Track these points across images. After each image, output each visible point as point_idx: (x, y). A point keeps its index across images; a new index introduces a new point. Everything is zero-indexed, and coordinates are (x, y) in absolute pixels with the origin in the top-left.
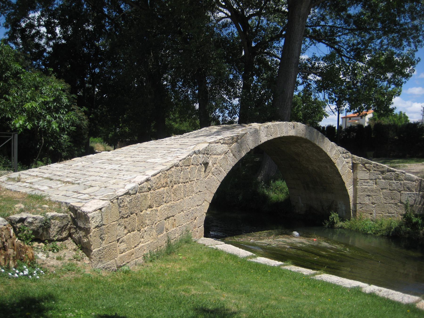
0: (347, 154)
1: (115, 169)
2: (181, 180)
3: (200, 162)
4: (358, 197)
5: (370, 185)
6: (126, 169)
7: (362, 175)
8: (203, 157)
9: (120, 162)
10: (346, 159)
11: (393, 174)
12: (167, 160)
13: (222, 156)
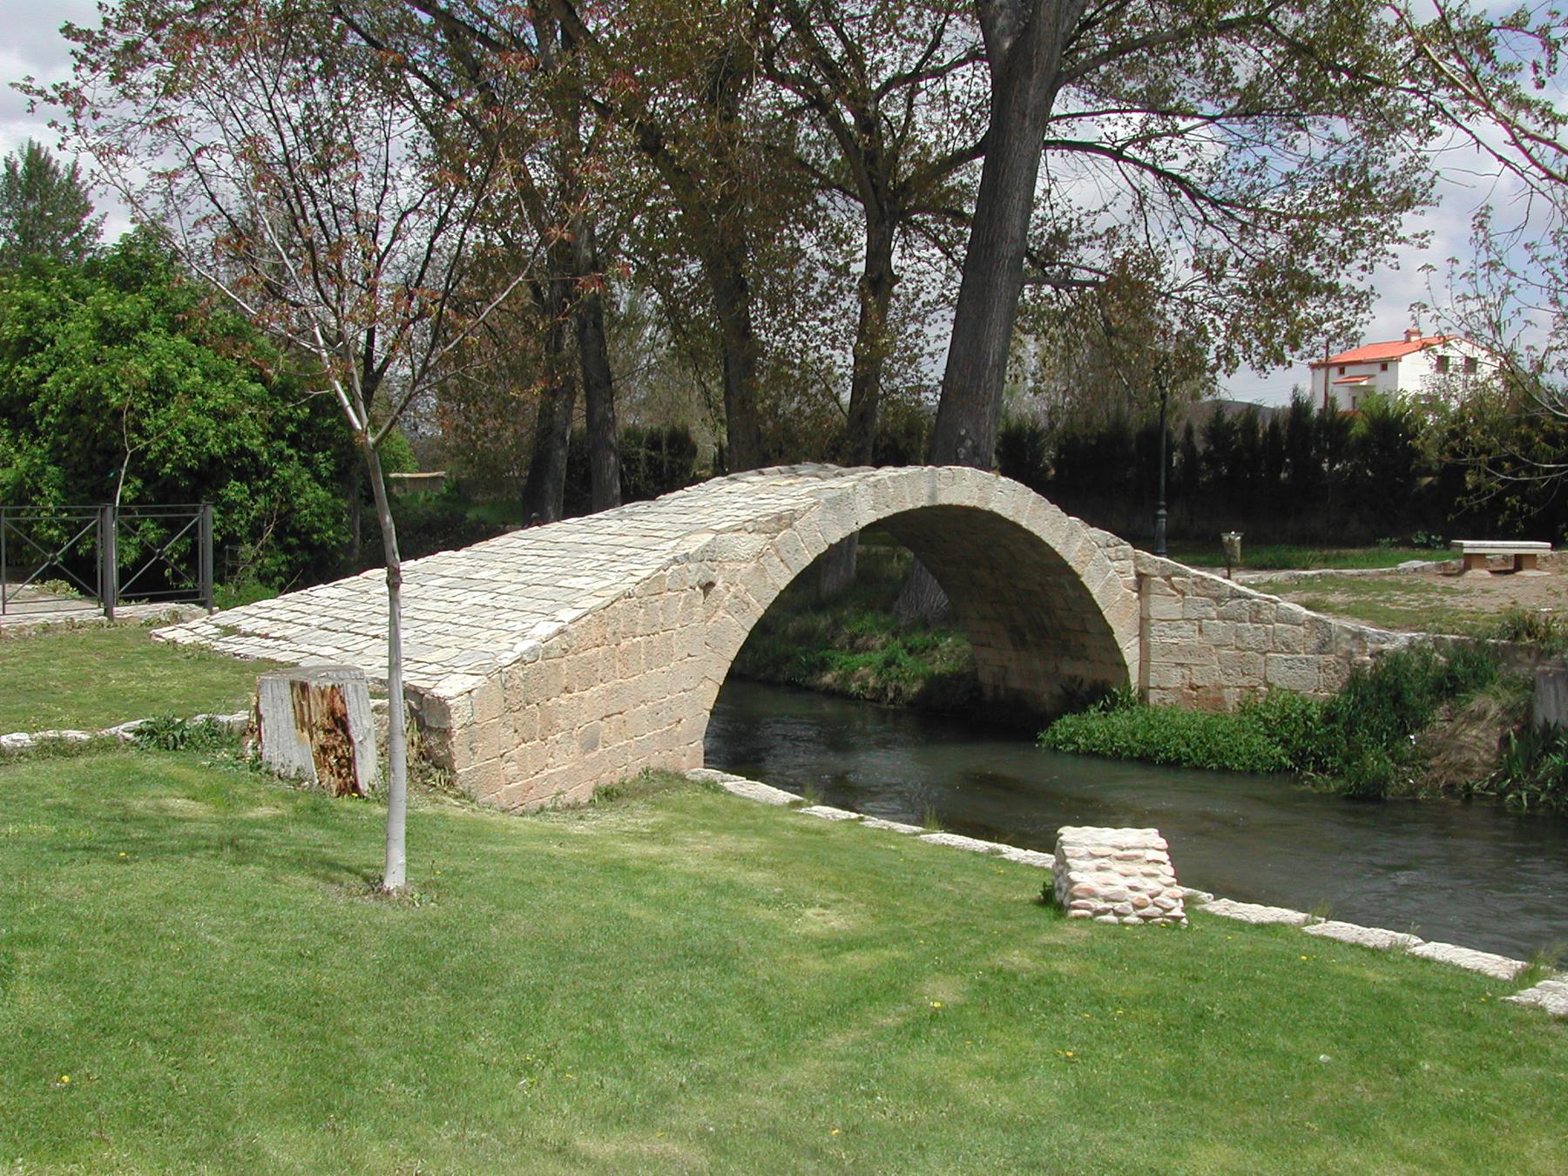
0: (1121, 547)
1: (484, 606)
2: (639, 630)
3: (690, 583)
4: (1152, 668)
5: (1185, 634)
6: (511, 605)
7: (1163, 606)
8: (699, 569)
9: (494, 585)
10: (1115, 564)
11: (1245, 603)
12: (606, 583)
13: (753, 564)
